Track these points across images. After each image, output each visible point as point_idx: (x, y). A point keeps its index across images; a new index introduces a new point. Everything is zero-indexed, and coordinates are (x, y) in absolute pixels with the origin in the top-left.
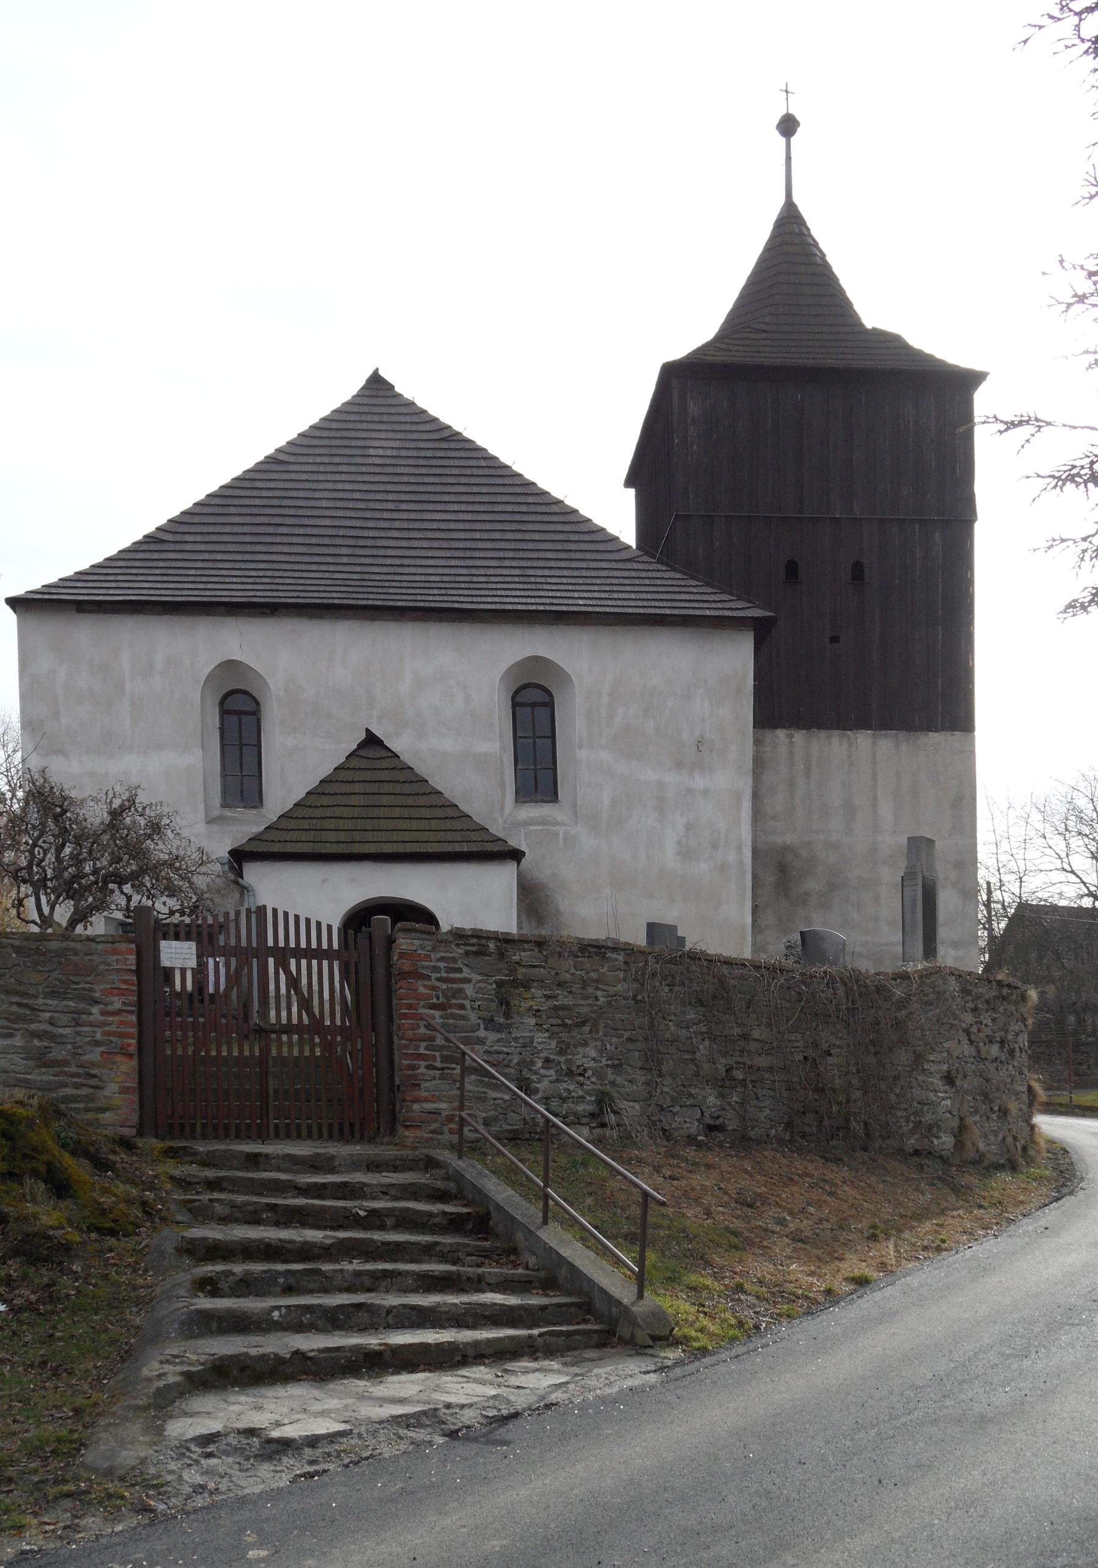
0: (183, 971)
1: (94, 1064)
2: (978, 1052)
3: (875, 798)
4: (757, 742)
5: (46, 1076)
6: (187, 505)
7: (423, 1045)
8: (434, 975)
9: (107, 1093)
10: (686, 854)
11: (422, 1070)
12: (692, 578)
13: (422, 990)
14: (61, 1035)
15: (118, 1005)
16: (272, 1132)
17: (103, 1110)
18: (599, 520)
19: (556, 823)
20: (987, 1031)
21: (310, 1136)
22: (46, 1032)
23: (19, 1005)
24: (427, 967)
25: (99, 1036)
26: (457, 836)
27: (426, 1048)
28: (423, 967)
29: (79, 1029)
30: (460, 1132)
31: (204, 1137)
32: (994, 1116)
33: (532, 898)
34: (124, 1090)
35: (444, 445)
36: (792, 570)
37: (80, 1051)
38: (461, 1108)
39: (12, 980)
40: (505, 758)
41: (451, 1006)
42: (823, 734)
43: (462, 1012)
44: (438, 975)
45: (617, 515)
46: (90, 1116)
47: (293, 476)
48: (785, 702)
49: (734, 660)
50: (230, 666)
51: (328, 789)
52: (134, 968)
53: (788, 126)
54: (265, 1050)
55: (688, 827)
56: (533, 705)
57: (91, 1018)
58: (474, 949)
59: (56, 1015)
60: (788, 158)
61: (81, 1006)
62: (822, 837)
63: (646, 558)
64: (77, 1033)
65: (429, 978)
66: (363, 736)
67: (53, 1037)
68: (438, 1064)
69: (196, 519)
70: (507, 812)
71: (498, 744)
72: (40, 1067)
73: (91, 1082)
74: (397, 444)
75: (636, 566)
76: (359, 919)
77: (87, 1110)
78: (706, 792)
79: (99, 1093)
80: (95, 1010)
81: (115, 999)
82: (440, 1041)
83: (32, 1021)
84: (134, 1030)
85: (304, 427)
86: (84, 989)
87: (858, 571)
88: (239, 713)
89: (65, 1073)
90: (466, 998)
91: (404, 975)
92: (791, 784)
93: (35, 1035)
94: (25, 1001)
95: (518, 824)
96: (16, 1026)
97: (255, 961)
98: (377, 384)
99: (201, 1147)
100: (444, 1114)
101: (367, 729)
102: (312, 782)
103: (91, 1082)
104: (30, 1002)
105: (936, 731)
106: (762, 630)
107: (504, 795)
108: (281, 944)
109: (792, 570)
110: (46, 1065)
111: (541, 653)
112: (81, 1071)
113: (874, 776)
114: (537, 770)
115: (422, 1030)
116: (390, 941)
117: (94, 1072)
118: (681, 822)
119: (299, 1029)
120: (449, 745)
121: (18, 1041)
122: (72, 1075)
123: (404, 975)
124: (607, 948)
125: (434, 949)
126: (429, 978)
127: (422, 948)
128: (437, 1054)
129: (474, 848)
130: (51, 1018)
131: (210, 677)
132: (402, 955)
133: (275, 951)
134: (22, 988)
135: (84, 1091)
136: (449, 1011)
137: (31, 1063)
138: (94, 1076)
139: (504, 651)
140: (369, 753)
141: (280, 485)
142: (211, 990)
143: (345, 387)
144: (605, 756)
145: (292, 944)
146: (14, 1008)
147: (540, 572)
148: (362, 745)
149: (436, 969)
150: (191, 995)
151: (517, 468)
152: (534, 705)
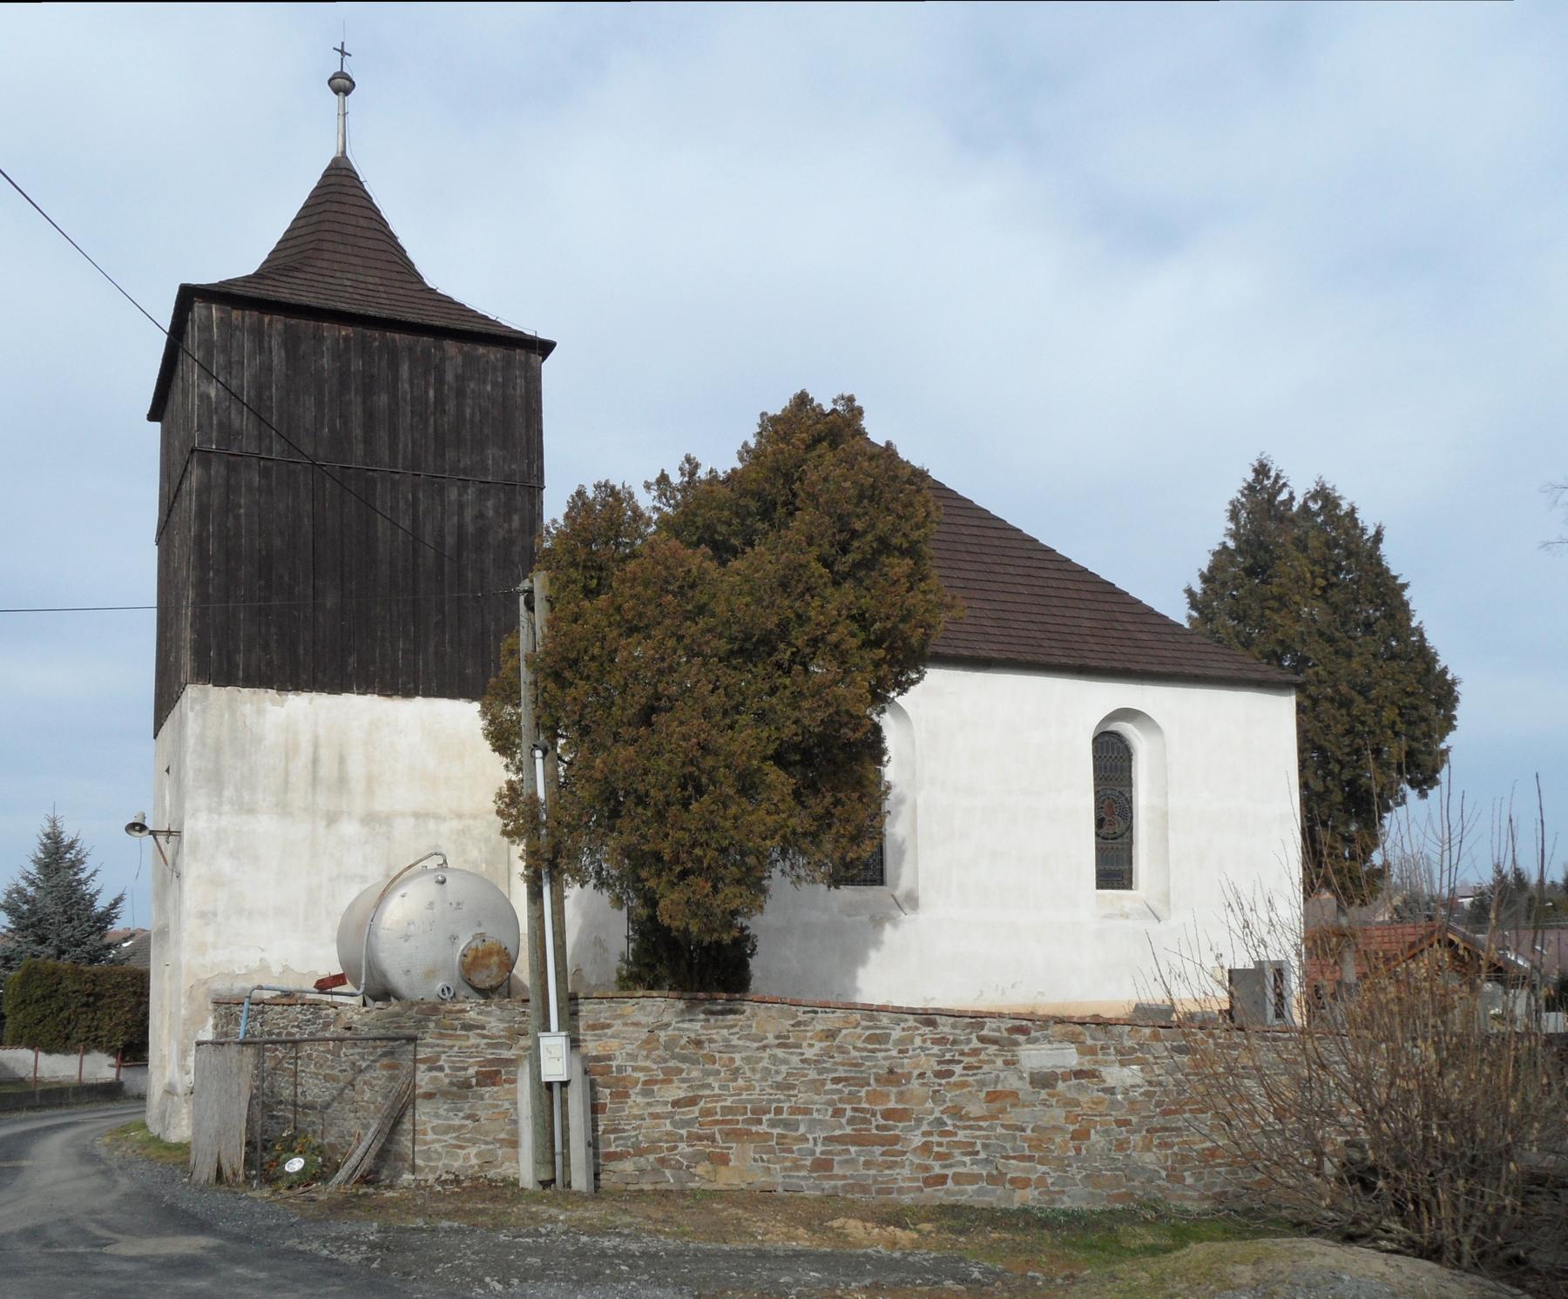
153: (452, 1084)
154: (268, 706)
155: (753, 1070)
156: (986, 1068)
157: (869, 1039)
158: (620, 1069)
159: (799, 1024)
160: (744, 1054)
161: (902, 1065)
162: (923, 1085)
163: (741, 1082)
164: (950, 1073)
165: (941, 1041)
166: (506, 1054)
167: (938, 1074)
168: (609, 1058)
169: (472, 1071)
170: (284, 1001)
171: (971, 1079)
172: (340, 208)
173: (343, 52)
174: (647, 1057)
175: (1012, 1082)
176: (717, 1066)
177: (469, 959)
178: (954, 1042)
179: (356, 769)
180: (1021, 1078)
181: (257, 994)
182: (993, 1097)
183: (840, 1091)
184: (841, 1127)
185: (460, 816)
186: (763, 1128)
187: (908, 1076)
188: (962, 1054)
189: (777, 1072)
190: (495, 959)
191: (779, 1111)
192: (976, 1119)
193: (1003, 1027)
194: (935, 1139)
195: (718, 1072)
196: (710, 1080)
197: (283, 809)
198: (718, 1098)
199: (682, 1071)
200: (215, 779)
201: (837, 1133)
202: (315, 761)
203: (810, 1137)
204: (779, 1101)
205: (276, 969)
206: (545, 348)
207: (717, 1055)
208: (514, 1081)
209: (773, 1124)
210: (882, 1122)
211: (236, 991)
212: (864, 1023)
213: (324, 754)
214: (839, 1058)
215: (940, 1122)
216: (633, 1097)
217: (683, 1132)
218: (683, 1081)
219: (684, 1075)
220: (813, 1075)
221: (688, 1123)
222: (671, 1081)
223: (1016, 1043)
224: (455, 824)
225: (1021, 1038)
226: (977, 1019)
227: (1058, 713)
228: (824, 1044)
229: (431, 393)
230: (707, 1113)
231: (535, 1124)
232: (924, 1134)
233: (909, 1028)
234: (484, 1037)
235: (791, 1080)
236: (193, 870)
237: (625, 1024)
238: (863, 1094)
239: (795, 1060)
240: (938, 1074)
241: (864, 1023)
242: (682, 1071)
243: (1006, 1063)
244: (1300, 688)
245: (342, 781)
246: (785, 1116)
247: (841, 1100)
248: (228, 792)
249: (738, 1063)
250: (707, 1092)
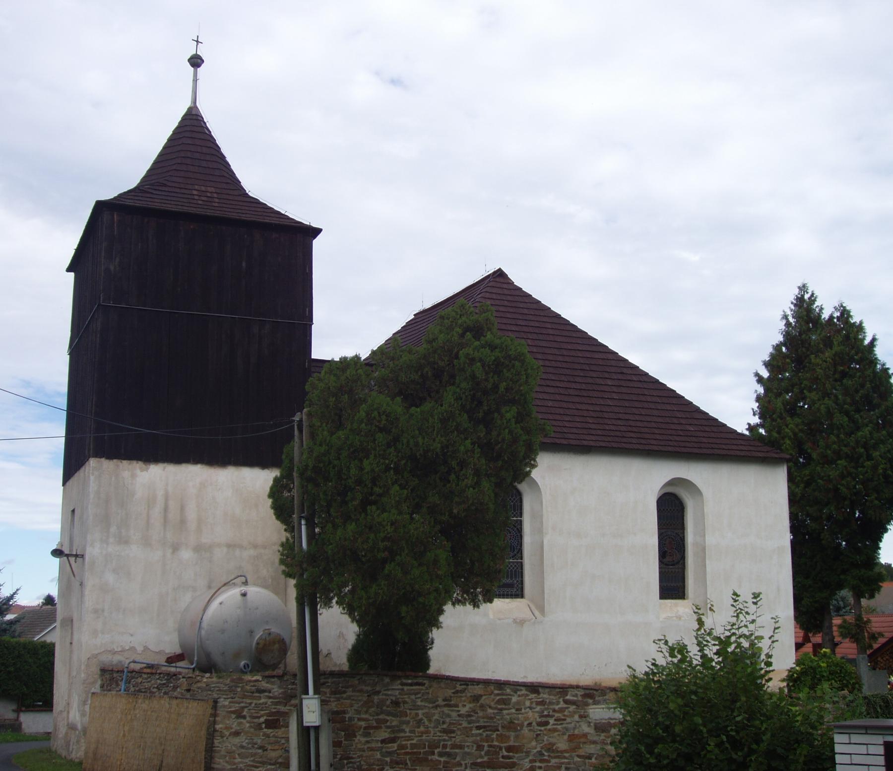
53: (196, 62)
60: (195, 80)
153: (251, 727)
154: (138, 472)
155: (430, 721)
156: (569, 720)
157: (498, 702)
158: (351, 719)
159: (457, 692)
160: (424, 711)
161: (518, 720)
162: (530, 730)
163: (422, 729)
164: (547, 723)
165: (542, 703)
166: (282, 708)
167: (540, 724)
168: (344, 712)
169: (262, 720)
170: (148, 671)
171: (559, 727)
172: (192, 146)
173: (197, 41)
174: (366, 712)
175: (585, 728)
176: (408, 718)
177: (261, 646)
178: (551, 703)
179: (191, 514)
180: (589, 726)
181: (132, 666)
182: (572, 738)
183: (481, 734)
184: (482, 757)
185: (255, 546)
186: (436, 757)
187: (522, 725)
188: (554, 711)
189: (444, 723)
190: (277, 646)
191: (445, 746)
192: (562, 752)
193: (579, 693)
194: (538, 764)
195: (408, 722)
196: (404, 727)
197: (146, 542)
198: (409, 738)
199: (387, 721)
200: (105, 520)
201: (479, 760)
202: (166, 509)
203: (463, 762)
204: (444, 740)
205: (140, 649)
206: (316, 232)
207: (408, 711)
208: (287, 727)
209: (441, 755)
210: (506, 754)
211: (114, 663)
212: (496, 692)
213: (171, 503)
214: (481, 714)
215: (541, 754)
216: (358, 737)
217: (388, 759)
218: (388, 727)
219: (388, 724)
220: (465, 724)
221: (389, 754)
222: (381, 728)
223: (587, 705)
224: (252, 552)
225: (590, 701)
226: (562, 689)
227: (629, 488)
228: (471, 705)
229: (244, 264)
230: (402, 747)
231: (299, 753)
232: (531, 761)
233: (522, 695)
234: (270, 698)
235: (453, 728)
236: (90, 582)
237: (353, 691)
238: (494, 736)
239: (454, 714)
240: (540, 724)
241: (496, 692)
242: (387, 721)
243: (581, 717)
244: (788, 461)
245: (183, 522)
246: (448, 750)
247: (482, 740)
248: (113, 529)
249: (420, 716)
250: (402, 734)
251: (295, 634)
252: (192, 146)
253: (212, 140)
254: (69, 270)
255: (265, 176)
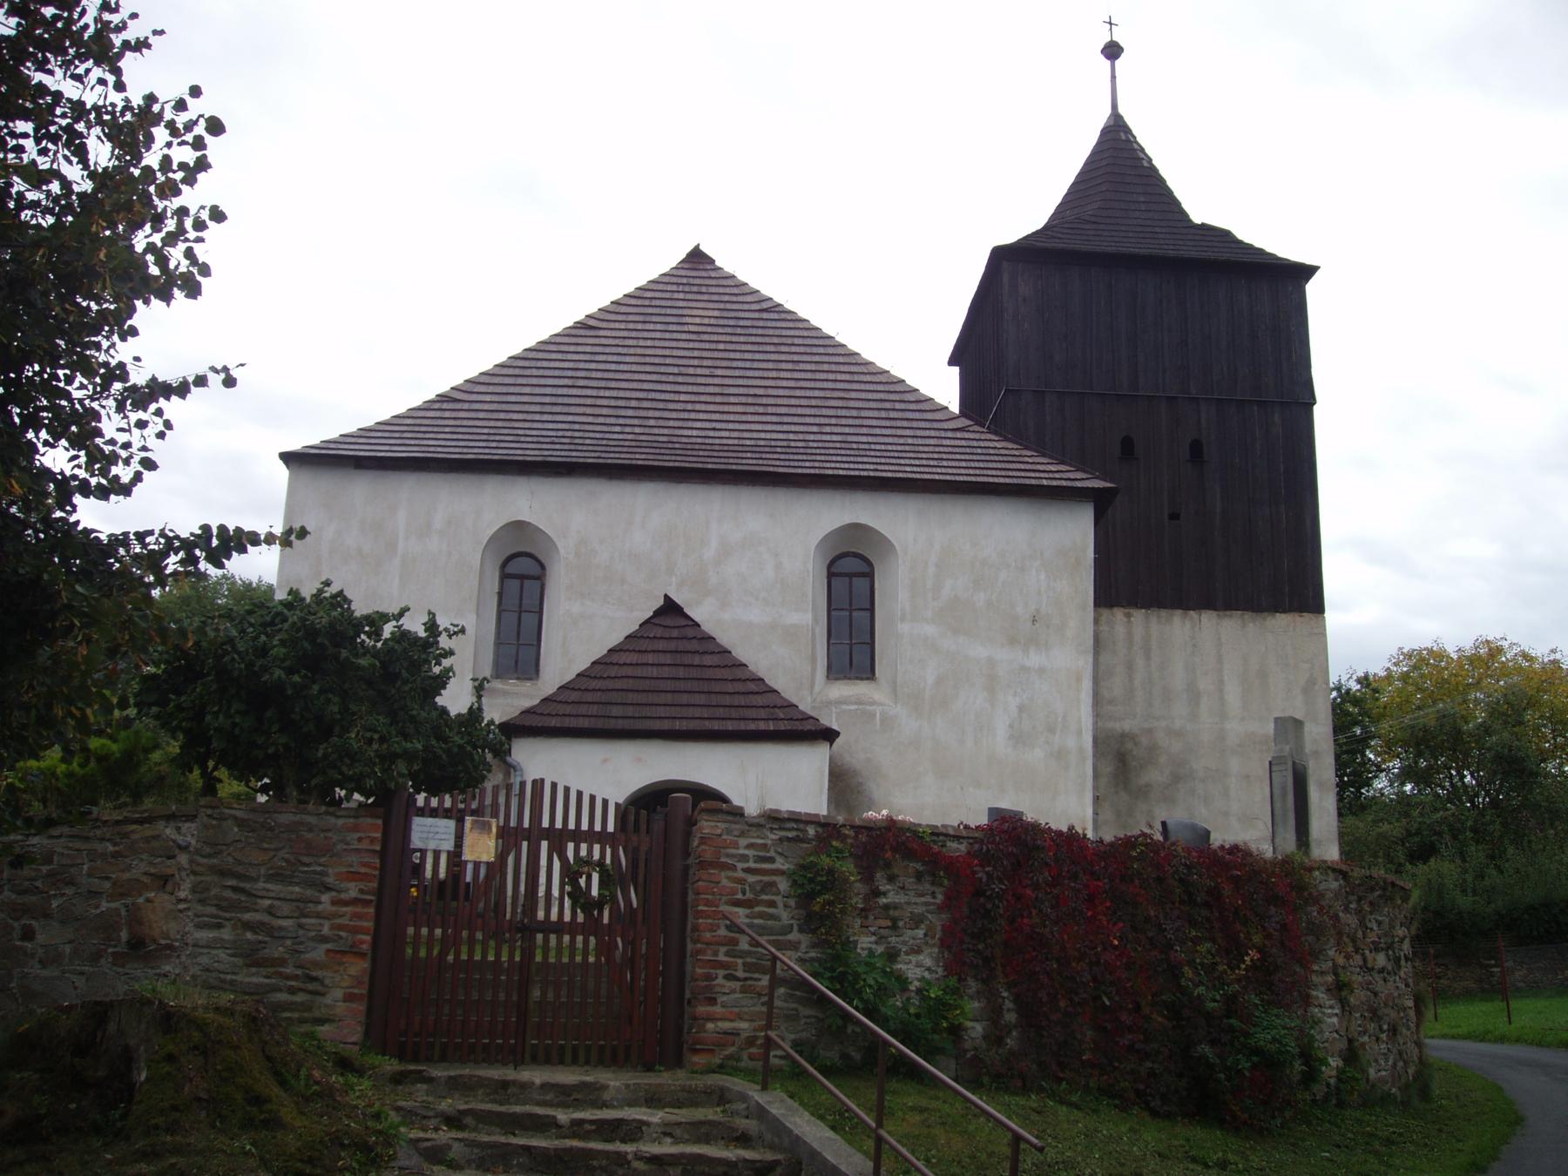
0: (437, 854)
1: (316, 964)
2: (1365, 960)
3: (1221, 681)
4: (1096, 621)
5: (256, 978)
6: (487, 366)
7: (723, 949)
8: (740, 865)
9: (328, 1000)
10: (1019, 738)
11: (720, 981)
12: (1026, 448)
13: (725, 882)
14: (281, 928)
15: (353, 894)
16: (527, 1056)
17: (321, 1021)
18: (926, 390)
19: (873, 703)
20: (1372, 937)
21: (575, 1061)
22: (263, 924)
23: (234, 889)
24: (733, 856)
25: (326, 931)
26: (763, 713)
27: (727, 954)
28: (728, 855)
29: (304, 920)
30: (766, 1058)
31: (443, 1058)
32: (1384, 1036)
33: (841, 782)
34: (349, 998)
35: (765, 315)
36: (1128, 446)
37: (301, 948)
38: (769, 1026)
39: (230, 859)
40: (817, 630)
41: (759, 903)
42: (1164, 613)
43: (771, 910)
44: (746, 865)
45: (943, 386)
46: (306, 1028)
47: (603, 341)
48: (1134, 577)
49: (1072, 534)
50: (519, 527)
51: (615, 658)
52: (378, 848)
53: (1112, 51)
54: (528, 953)
55: (1021, 708)
56: (851, 575)
57: (320, 908)
58: (791, 834)
59: (277, 903)
60: (1113, 77)
61: (309, 892)
62: (1164, 724)
63: (977, 428)
64: (301, 926)
65: (734, 868)
66: (661, 602)
67: (270, 931)
68: (740, 974)
69: (496, 380)
70: (817, 688)
71: (810, 616)
72: (248, 966)
73: (310, 986)
74: (716, 313)
75: (966, 435)
76: (652, 801)
77: (302, 1021)
78: (1041, 671)
79: (319, 999)
80: (325, 898)
81: (352, 885)
82: (744, 945)
83: (248, 910)
84: (370, 924)
85: (618, 295)
86: (315, 872)
87: (1196, 450)
88: (521, 572)
89: (281, 974)
90: (778, 893)
91: (703, 865)
92: (1130, 667)
93: (248, 926)
94: (242, 885)
95: (829, 703)
96: (227, 915)
97: (525, 844)
98: (697, 258)
99: (439, 1072)
100: (744, 1035)
101: (666, 596)
102: (599, 651)
103: (310, 986)
104: (247, 886)
105: (1284, 612)
106: (1101, 502)
107: (814, 670)
108: (559, 825)
109: (1128, 446)
110: (257, 964)
111: (863, 519)
112: (299, 972)
113: (1220, 660)
114: (852, 644)
115: (722, 932)
116: (691, 823)
117: (314, 974)
118: (1013, 703)
119: (572, 928)
120: (755, 615)
121: (226, 934)
122: (288, 978)
123: (703, 865)
124: (946, 835)
125: (742, 834)
126: (734, 868)
127: (729, 832)
128: (740, 961)
129: (782, 726)
130: (271, 906)
131: (494, 539)
132: (703, 840)
133: (550, 833)
134: (240, 869)
135: (300, 998)
136: (757, 909)
137: (239, 961)
138: (315, 979)
139: (827, 515)
140: (668, 621)
141: (588, 349)
142: (469, 878)
143: (668, 258)
144: (930, 630)
145: (572, 826)
146: (228, 894)
147: (864, 439)
148: (658, 613)
149: (744, 858)
150: (442, 884)
151: (840, 339)
152: (850, 575)
206: (1308, 271)
251: (884, 1156)
252: (1119, 169)
253: (1169, 193)
254: (952, 362)
255: (1215, 191)
